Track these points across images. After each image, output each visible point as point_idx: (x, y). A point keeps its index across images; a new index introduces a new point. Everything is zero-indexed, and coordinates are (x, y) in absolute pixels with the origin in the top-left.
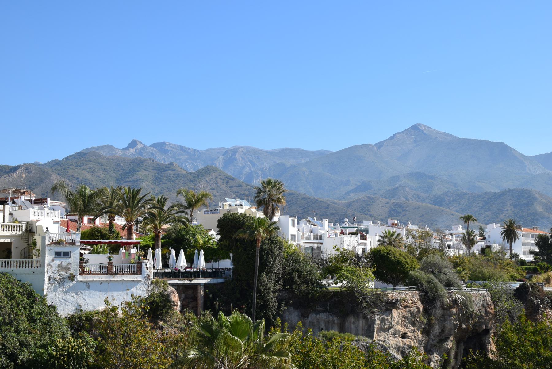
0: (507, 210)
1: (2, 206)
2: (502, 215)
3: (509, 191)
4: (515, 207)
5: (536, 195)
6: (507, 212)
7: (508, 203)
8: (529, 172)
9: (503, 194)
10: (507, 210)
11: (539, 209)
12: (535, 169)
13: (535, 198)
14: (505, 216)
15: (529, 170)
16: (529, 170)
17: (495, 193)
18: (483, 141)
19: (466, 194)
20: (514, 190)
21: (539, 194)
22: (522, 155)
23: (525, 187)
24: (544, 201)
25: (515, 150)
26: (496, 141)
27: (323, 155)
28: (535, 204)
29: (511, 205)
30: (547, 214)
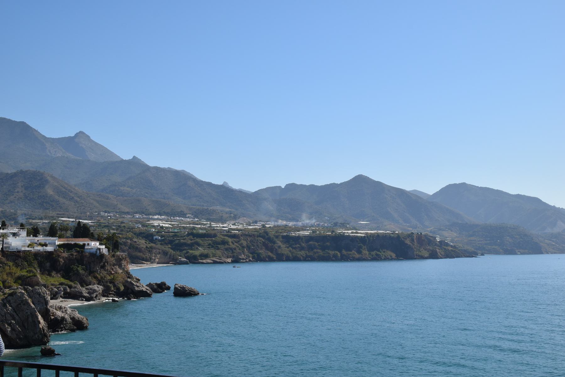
0: (18, 192)
1: (6, 369)
2: (12, 197)
3: (22, 172)
4: (26, 189)
5: (48, 177)
6: (17, 194)
7: (20, 184)
8: (49, 154)
9: (15, 175)
10: (18, 192)
11: (50, 192)
12: (55, 152)
13: (47, 181)
14: (15, 197)
15: (50, 152)
16: (50, 152)
17: (7, 174)
18: (5, 119)
19: (447, 245)
20: (26, 171)
21: (52, 177)
22: (44, 136)
23: (42, 171)
24: (55, 184)
25: (36, 131)
26: (18, 120)
27: (312, 188)
28: (47, 187)
29: (22, 186)
30: (57, 197)
